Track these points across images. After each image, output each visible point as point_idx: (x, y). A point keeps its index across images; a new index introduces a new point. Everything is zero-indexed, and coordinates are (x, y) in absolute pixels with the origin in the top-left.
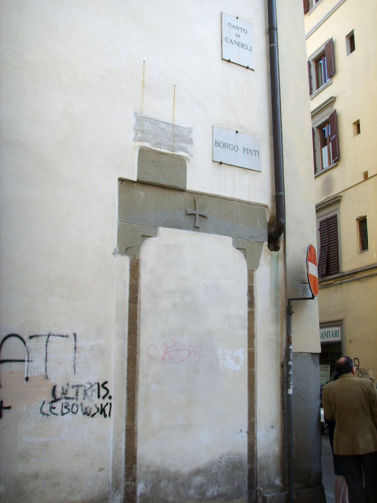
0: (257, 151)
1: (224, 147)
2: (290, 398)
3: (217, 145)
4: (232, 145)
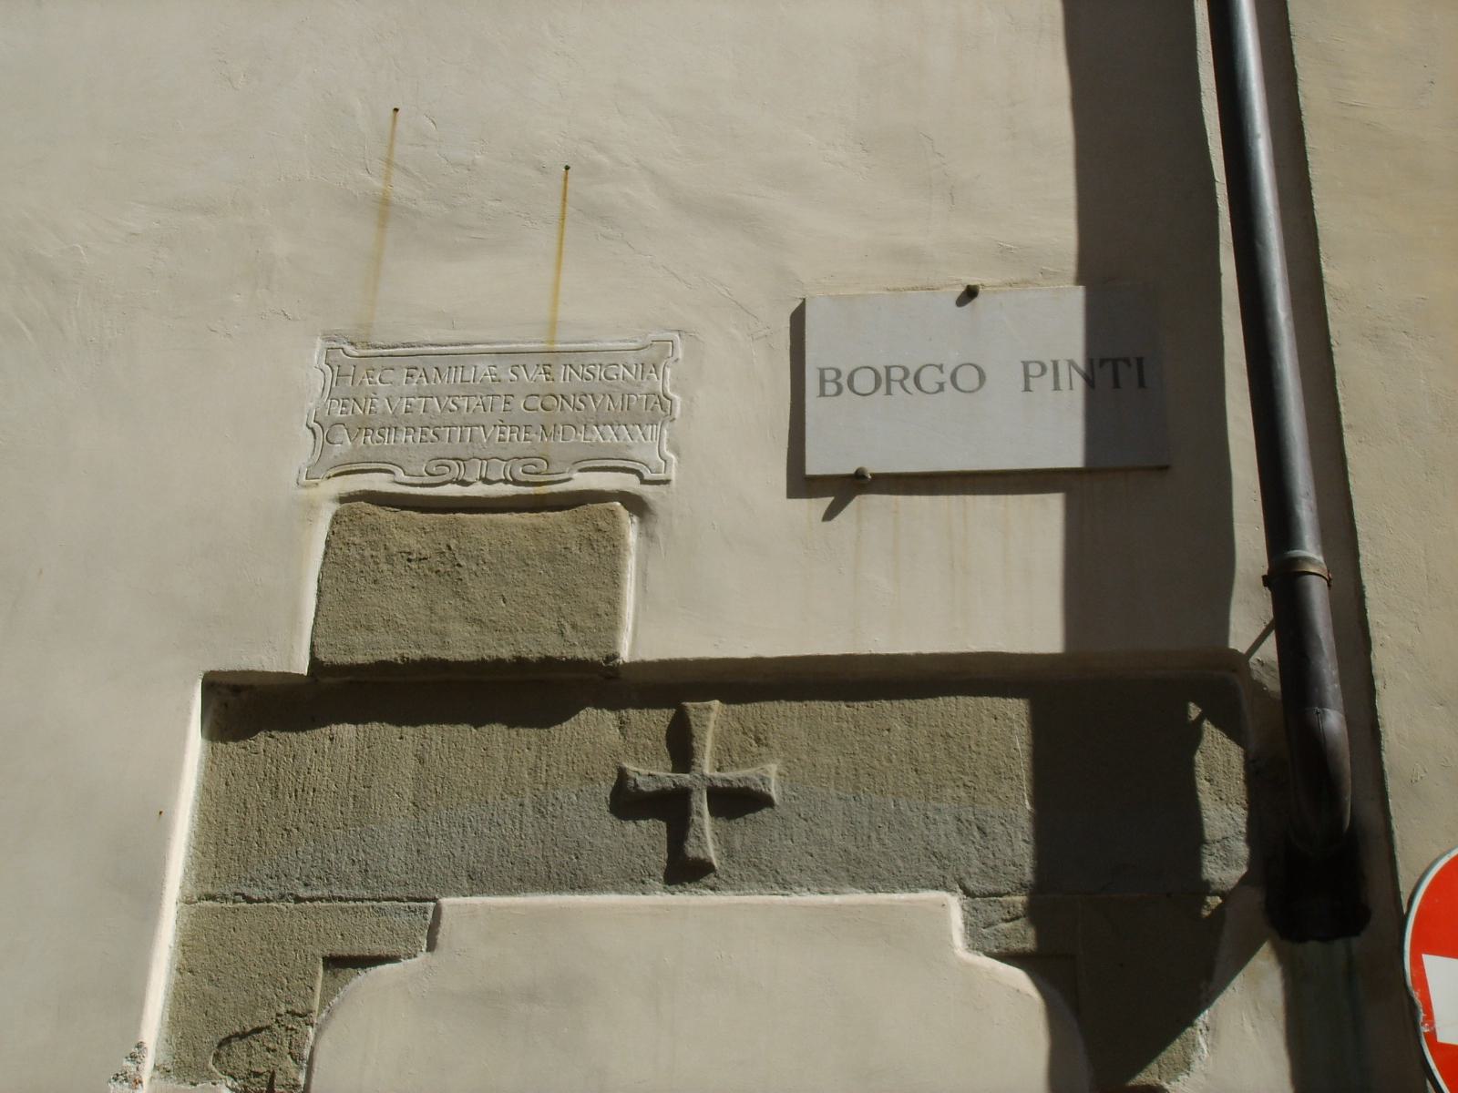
0: (1127, 361)
1: (883, 386)
2: (1336, 686)
3: (831, 388)
4: (941, 368)
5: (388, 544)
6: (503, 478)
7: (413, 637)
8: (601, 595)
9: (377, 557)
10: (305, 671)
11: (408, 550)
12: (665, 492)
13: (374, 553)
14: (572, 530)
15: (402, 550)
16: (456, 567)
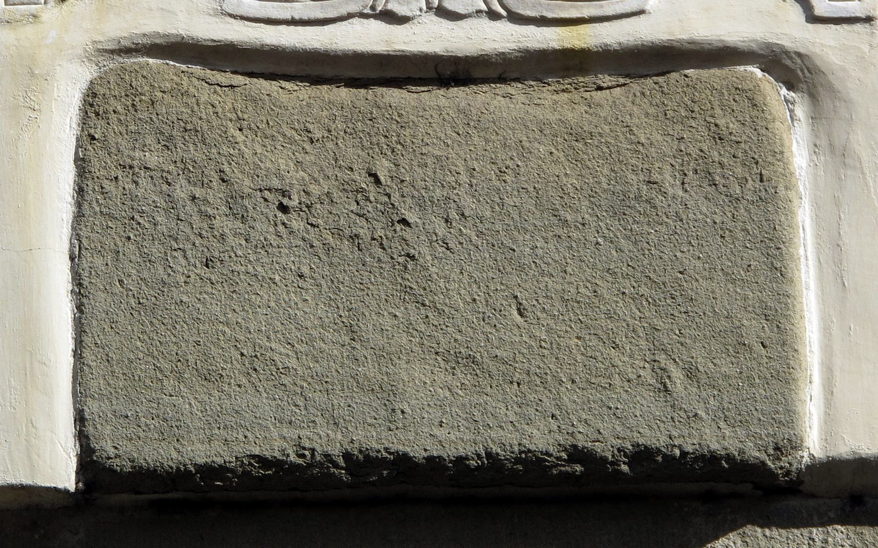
5: (226, 167)
6: (484, 7)
7: (319, 398)
8: (746, 298)
9: (205, 200)
10: (71, 486)
11: (276, 183)
12: (866, 48)
13: (198, 192)
14: (657, 137)
15: (263, 184)
16: (398, 227)
